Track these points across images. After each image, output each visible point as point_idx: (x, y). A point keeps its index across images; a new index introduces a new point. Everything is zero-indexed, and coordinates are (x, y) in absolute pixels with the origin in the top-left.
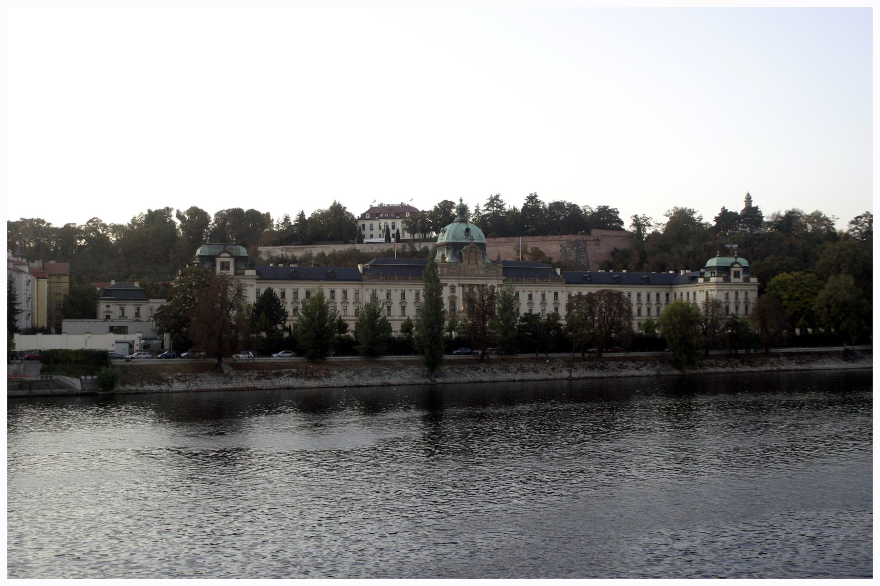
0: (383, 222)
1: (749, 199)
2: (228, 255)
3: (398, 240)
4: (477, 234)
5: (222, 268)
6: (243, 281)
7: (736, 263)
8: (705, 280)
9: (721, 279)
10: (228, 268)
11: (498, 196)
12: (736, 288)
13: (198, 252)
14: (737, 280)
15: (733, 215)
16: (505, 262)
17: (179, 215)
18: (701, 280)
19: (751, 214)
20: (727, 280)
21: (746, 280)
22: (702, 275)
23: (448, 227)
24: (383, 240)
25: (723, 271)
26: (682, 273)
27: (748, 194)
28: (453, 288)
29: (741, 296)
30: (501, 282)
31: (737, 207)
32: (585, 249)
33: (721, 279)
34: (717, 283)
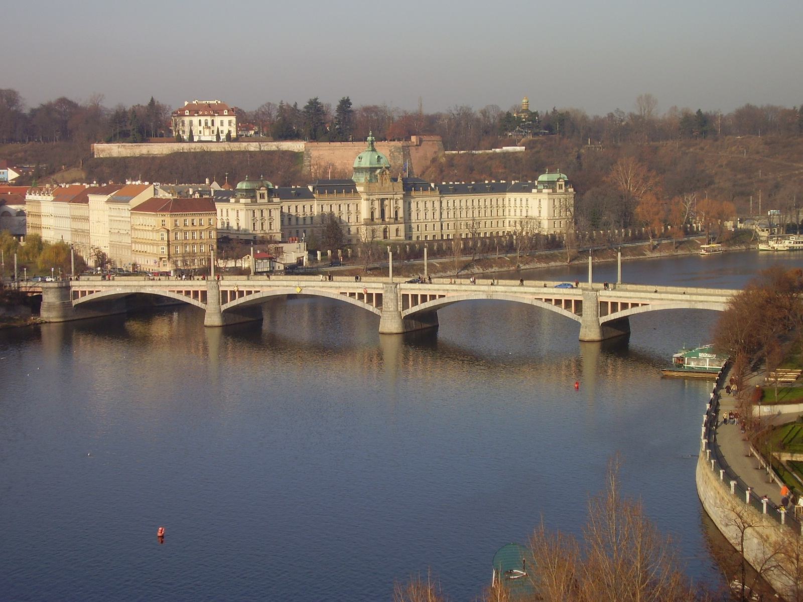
0: (203, 119)
8: (537, 191)
9: (249, 200)
10: (263, 198)
12: (262, 207)
14: (262, 201)
20: (554, 191)
21: (566, 190)
22: (536, 187)
25: (550, 184)
28: (397, 200)
34: (549, 194)
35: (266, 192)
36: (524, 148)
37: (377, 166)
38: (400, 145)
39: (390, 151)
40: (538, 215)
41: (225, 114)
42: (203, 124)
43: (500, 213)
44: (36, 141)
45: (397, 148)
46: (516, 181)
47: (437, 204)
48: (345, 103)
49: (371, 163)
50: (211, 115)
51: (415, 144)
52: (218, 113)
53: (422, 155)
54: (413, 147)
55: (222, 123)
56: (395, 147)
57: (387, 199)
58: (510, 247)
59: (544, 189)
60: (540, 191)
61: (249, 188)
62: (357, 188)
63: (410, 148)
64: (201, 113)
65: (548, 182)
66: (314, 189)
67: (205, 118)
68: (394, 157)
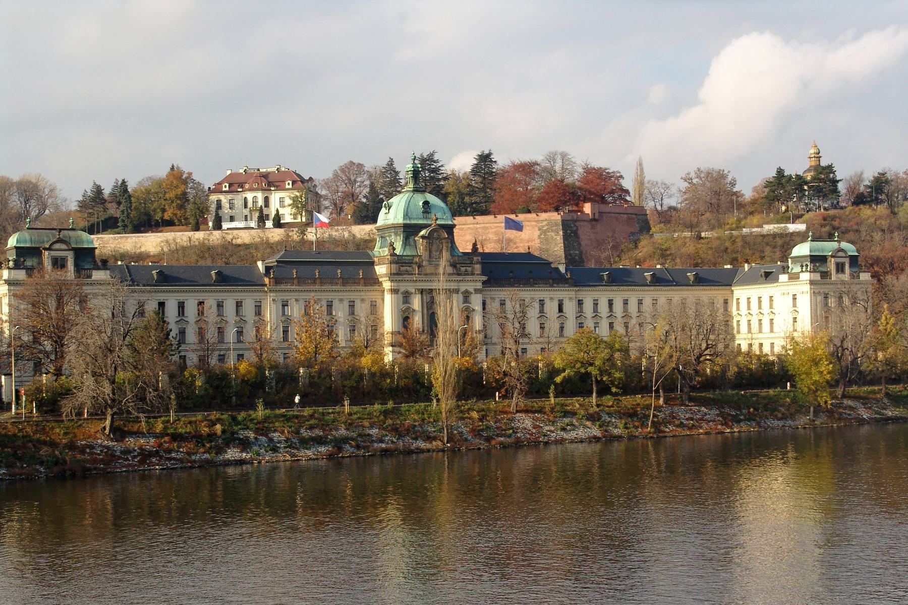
0: (250, 196)
1: (95, 184)
2: (64, 247)
3: (278, 224)
6: (87, 289)
8: (790, 278)
10: (843, 271)
11: (432, 155)
13: (12, 242)
16: (485, 255)
18: (783, 278)
22: (785, 270)
23: (395, 200)
28: (466, 296)
29: (633, 307)
30: (479, 285)
31: (798, 165)
33: (817, 276)
37: (421, 222)
39: (540, 229)
40: (792, 329)
41: (287, 187)
44: (615, 394)
45: (551, 224)
48: (485, 159)
49: (406, 215)
50: (263, 190)
52: (277, 187)
54: (585, 223)
55: (282, 200)
58: (635, 382)
59: (802, 271)
60: (794, 277)
61: (28, 245)
63: (578, 224)
64: (247, 186)
66: (268, 269)
68: (547, 239)
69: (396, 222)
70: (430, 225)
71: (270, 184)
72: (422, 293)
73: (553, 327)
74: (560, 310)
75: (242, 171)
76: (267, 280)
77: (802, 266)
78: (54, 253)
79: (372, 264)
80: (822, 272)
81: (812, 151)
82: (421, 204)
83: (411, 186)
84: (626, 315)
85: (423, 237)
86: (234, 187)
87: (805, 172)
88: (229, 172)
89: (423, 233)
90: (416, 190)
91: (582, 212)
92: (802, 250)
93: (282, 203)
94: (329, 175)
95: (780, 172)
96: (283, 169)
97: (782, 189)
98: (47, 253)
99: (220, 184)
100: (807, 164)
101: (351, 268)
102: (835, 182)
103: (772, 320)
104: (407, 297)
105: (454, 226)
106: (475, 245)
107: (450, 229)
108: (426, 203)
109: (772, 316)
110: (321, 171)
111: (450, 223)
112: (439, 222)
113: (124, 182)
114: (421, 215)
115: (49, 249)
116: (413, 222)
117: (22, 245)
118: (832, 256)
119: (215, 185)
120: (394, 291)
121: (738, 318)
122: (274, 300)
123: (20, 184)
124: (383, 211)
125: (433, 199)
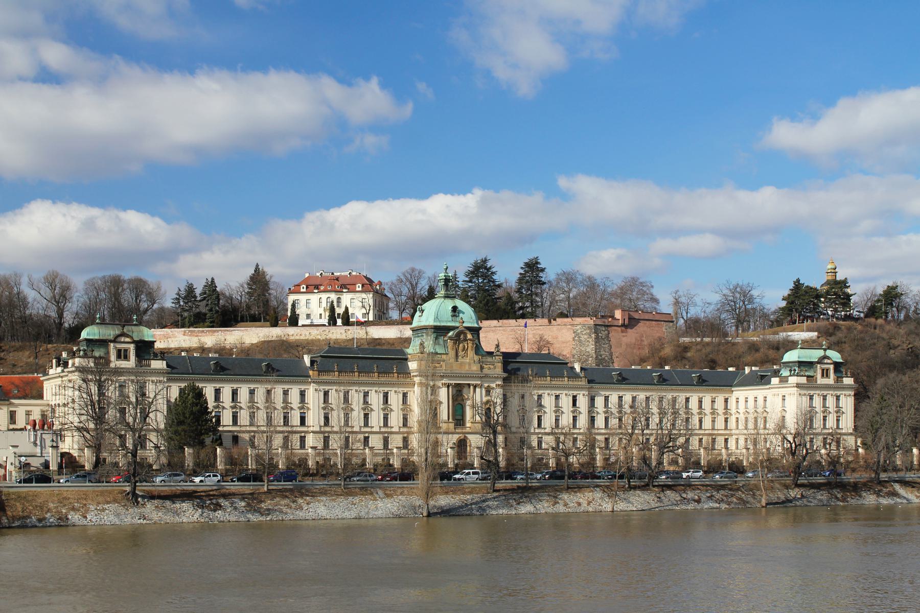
2: (128, 340)
4: (468, 315)
5: (119, 357)
7: (825, 357)
8: (780, 381)
10: (126, 358)
14: (123, 364)
15: (815, 294)
17: (32, 285)
18: (775, 381)
19: (838, 291)
22: (776, 373)
24: (325, 321)
26: (747, 370)
27: (257, 265)
32: (608, 336)
35: (132, 347)
36: (816, 334)
38: (592, 322)
41: (358, 289)
42: (324, 304)
43: (720, 424)
46: (753, 368)
47: (583, 402)
48: (533, 267)
49: (436, 318)
50: (336, 291)
51: (620, 322)
53: (633, 341)
56: (584, 325)
57: (469, 385)
61: (97, 337)
62: (409, 363)
64: (322, 288)
65: (801, 364)
66: (312, 362)
67: (328, 295)
69: (427, 324)
70: (458, 327)
71: (343, 286)
72: (448, 387)
73: (566, 420)
74: (574, 404)
75: (318, 274)
76: (311, 373)
77: (791, 371)
78: (119, 346)
79: (406, 359)
80: (808, 377)
81: (830, 266)
82: (450, 308)
83: (443, 292)
84: (714, 412)
85: (450, 338)
86: (311, 288)
87: (822, 286)
88: (307, 275)
89: (451, 334)
90: (447, 297)
91: (613, 317)
92: (791, 356)
93: (357, 304)
94: (394, 278)
95: (798, 285)
96: (354, 273)
97: (802, 303)
98: (112, 344)
99: (299, 285)
100: (825, 278)
101: (387, 363)
102: (848, 297)
103: (765, 418)
104: (434, 390)
105: (480, 328)
106: (498, 346)
107: (476, 331)
108: (455, 309)
109: (765, 414)
110: (387, 275)
111: (476, 325)
112: (464, 325)
113: (213, 279)
114: (450, 318)
115: (114, 341)
116: (443, 324)
117: (91, 337)
118: (818, 363)
119: (295, 286)
120: (421, 384)
121: (737, 415)
122: (316, 390)
123: (130, 281)
124: (418, 314)
125: (461, 305)
